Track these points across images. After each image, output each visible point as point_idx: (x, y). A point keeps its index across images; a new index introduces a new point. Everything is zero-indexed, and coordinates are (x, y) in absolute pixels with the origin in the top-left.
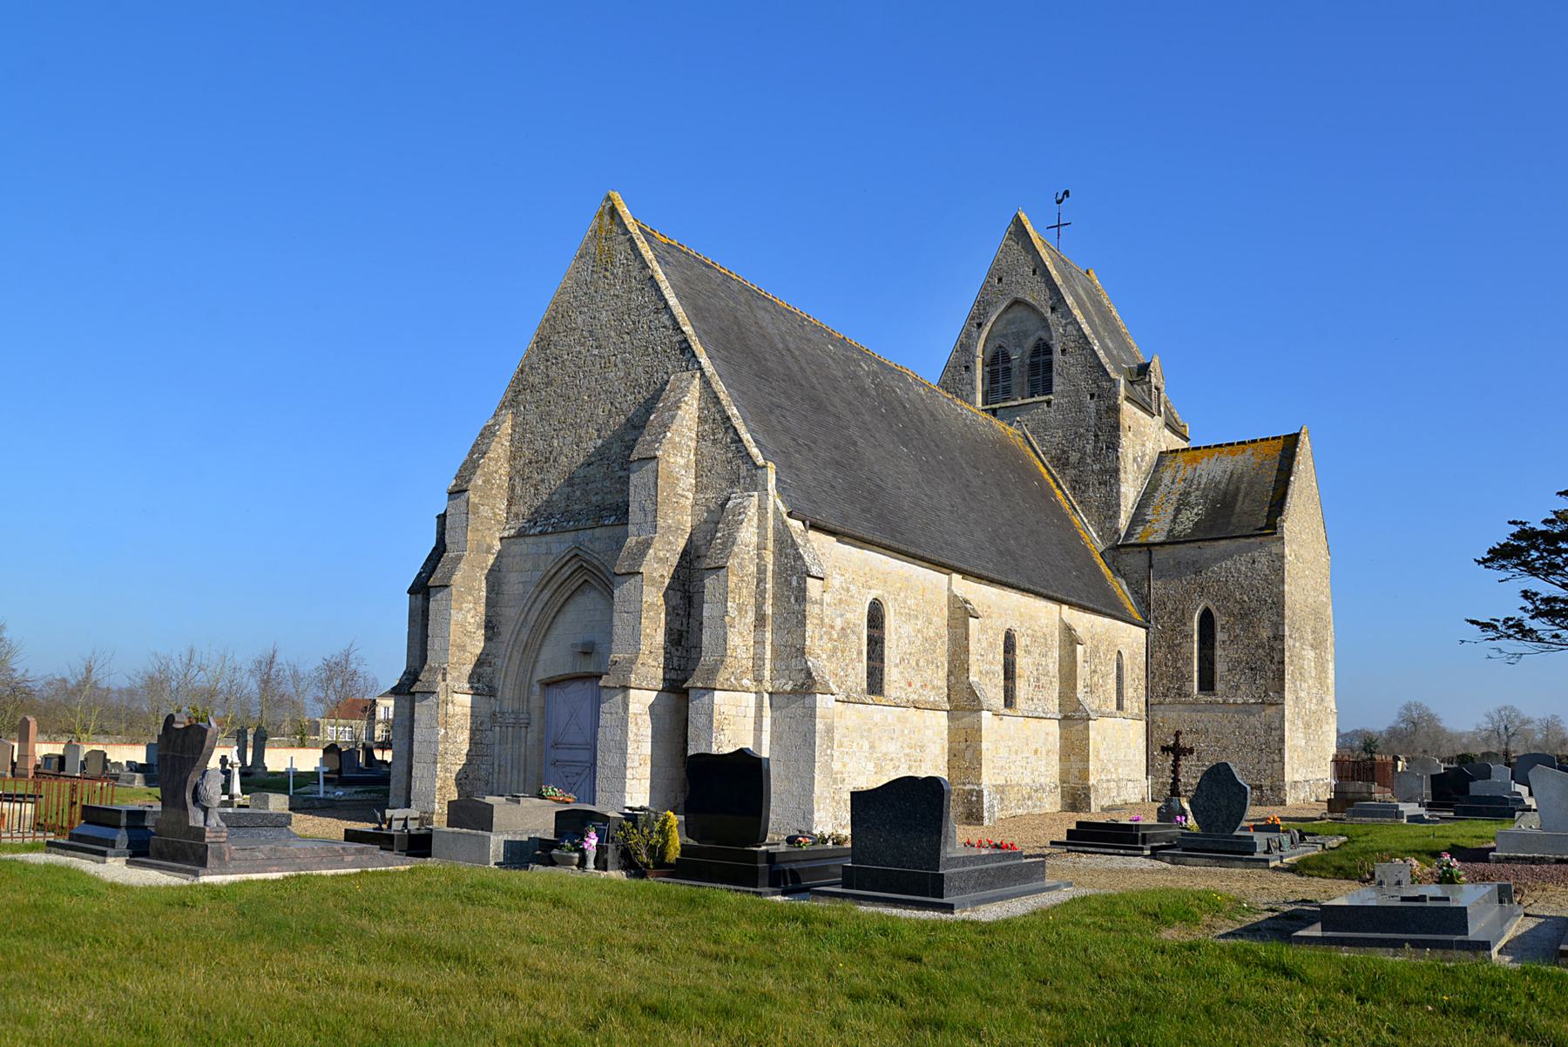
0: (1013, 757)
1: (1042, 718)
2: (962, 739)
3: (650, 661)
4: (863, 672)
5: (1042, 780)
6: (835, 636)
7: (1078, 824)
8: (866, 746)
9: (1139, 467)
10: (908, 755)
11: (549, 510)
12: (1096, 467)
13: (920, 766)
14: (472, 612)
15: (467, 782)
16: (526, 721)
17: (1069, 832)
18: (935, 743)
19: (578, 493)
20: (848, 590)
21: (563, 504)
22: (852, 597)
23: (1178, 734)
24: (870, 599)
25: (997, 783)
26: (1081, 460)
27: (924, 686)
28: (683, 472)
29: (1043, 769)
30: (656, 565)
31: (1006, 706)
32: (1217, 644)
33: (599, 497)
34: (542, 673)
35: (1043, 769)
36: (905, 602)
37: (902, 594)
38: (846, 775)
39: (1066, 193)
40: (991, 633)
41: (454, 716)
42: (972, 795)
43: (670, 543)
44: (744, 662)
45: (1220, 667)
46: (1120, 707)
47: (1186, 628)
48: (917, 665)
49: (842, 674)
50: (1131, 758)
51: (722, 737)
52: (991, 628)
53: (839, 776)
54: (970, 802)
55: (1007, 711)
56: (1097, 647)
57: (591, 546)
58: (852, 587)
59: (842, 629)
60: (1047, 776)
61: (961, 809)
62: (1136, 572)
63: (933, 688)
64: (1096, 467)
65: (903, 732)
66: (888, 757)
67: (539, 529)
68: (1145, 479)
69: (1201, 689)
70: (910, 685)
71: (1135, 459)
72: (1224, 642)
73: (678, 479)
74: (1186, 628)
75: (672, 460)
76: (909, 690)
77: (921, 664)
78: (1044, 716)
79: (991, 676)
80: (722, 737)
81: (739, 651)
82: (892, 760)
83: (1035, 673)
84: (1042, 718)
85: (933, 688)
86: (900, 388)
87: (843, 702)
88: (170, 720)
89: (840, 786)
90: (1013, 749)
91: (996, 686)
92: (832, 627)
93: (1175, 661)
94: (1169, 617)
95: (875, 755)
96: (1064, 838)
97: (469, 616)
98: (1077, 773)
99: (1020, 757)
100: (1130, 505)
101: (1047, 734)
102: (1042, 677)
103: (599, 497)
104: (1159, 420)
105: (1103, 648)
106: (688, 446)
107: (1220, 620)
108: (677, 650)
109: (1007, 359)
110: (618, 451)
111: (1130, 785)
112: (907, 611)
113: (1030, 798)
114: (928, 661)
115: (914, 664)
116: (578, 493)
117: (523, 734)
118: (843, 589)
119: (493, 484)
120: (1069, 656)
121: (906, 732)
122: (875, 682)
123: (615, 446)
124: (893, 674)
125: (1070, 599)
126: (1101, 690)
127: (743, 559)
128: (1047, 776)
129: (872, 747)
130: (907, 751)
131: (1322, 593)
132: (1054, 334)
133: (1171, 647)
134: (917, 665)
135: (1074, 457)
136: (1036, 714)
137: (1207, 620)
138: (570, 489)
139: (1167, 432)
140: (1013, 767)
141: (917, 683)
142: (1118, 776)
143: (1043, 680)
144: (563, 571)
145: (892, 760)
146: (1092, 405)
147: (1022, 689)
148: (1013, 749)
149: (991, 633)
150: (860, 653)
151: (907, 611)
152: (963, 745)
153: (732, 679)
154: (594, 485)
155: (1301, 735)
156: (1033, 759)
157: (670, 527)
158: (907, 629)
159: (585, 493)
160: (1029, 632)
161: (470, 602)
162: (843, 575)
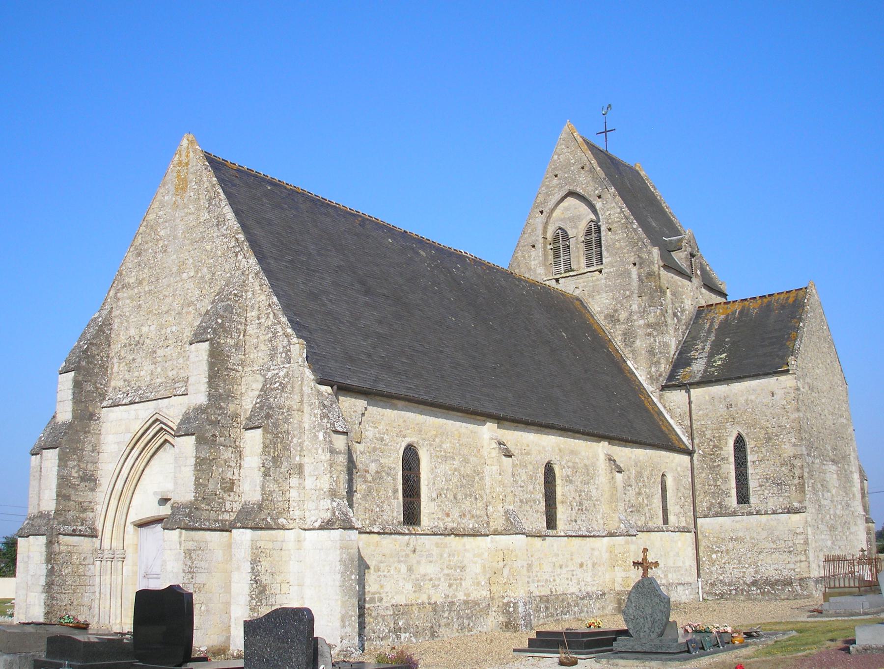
0: (558, 571)
1: (586, 536)
2: (500, 559)
3: (203, 506)
4: (398, 507)
5: (589, 589)
6: (370, 479)
7: (538, 633)
8: (404, 568)
9: (679, 320)
10: (448, 575)
11: (138, 384)
12: (641, 322)
13: (461, 584)
14: (76, 468)
15: (72, 608)
16: (122, 556)
17: (531, 641)
18: (475, 563)
19: (159, 369)
20: (382, 440)
21: (148, 379)
22: (386, 445)
23: (645, 550)
24: (404, 445)
25: (542, 594)
26: (629, 319)
27: (462, 516)
28: (234, 350)
29: (589, 579)
30: (207, 427)
31: (548, 528)
32: (749, 464)
33: (174, 372)
34: (134, 516)
35: (589, 579)
36: (441, 446)
37: (437, 440)
38: (383, 595)
39: (610, 105)
40: (530, 467)
41: (60, 553)
42: (510, 607)
43: (221, 408)
44: (280, 504)
45: (753, 484)
46: (666, 521)
47: (723, 453)
48: (455, 498)
49: (378, 509)
50: (680, 564)
51: (259, 568)
52: (531, 463)
53: (376, 596)
54: (508, 612)
55: (551, 532)
56: (640, 473)
57: (167, 412)
58: (386, 437)
59: (377, 472)
60: (593, 585)
61: (501, 618)
62: (679, 408)
63: (473, 516)
64: (641, 322)
65: (442, 556)
66: (428, 578)
67: (130, 399)
68: (686, 329)
69: (739, 502)
70: (448, 515)
71: (675, 315)
72: (754, 462)
73: (228, 356)
74: (723, 453)
75: (222, 341)
76: (447, 519)
77: (459, 496)
78: (588, 534)
79: (532, 503)
80: (259, 568)
81: (274, 495)
82: (431, 580)
83: (577, 498)
84: (586, 536)
85: (473, 516)
86: (457, 268)
87: (379, 533)
88: (551, 460)
89: (378, 604)
90: (557, 565)
91: (537, 511)
92: (367, 471)
93: (715, 480)
94: (708, 444)
95: (413, 577)
96: (526, 645)
97: (73, 471)
98: (621, 582)
99: (564, 570)
100: (672, 353)
101: (593, 549)
102: (584, 502)
103: (174, 372)
104: (696, 281)
105: (646, 474)
106: (238, 329)
107: (750, 445)
108: (229, 496)
109: (566, 237)
110: (189, 335)
111: (680, 588)
112: (442, 453)
113: (577, 605)
114: (466, 496)
115: (452, 497)
116: (159, 369)
117: (120, 567)
118: (377, 439)
119: (95, 365)
120: (610, 482)
121: (445, 555)
122: (411, 515)
123: (187, 330)
124: (427, 507)
125: (611, 434)
126: (646, 509)
127: (277, 419)
128: (593, 585)
129: (410, 570)
130: (446, 571)
131: (842, 416)
132: (601, 217)
133: (712, 468)
134: (455, 498)
135: (623, 316)
136: (580, 533)
137: (740, 443)
138: (153, 366)
139: (704, 291)
140: (558, 581)
141: (455, 513)
142: (668, 581)
143: (586, 504)
144: (148, 432)
145: (431, 580)
146: (634, 271)
147: (562, 513)
148: (557, 565)
149: (530, 467)
150: (395, 491)
151: (442, 453)
152: (501, 564)
153: (269, 520)
154: (171, 363)
155: (827, 537)
156: (579, 571)
157: (221, 395)
158: (444, 468)
159: (164, 369)
160: (570, 464)
161: (74, 460)
162: (376, 427)
